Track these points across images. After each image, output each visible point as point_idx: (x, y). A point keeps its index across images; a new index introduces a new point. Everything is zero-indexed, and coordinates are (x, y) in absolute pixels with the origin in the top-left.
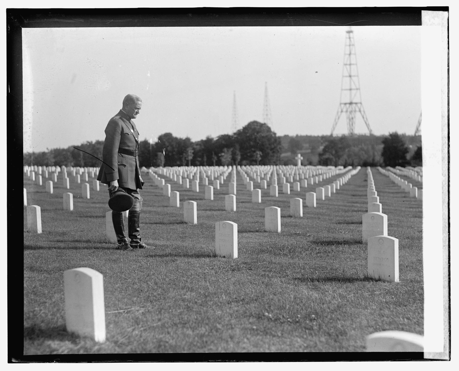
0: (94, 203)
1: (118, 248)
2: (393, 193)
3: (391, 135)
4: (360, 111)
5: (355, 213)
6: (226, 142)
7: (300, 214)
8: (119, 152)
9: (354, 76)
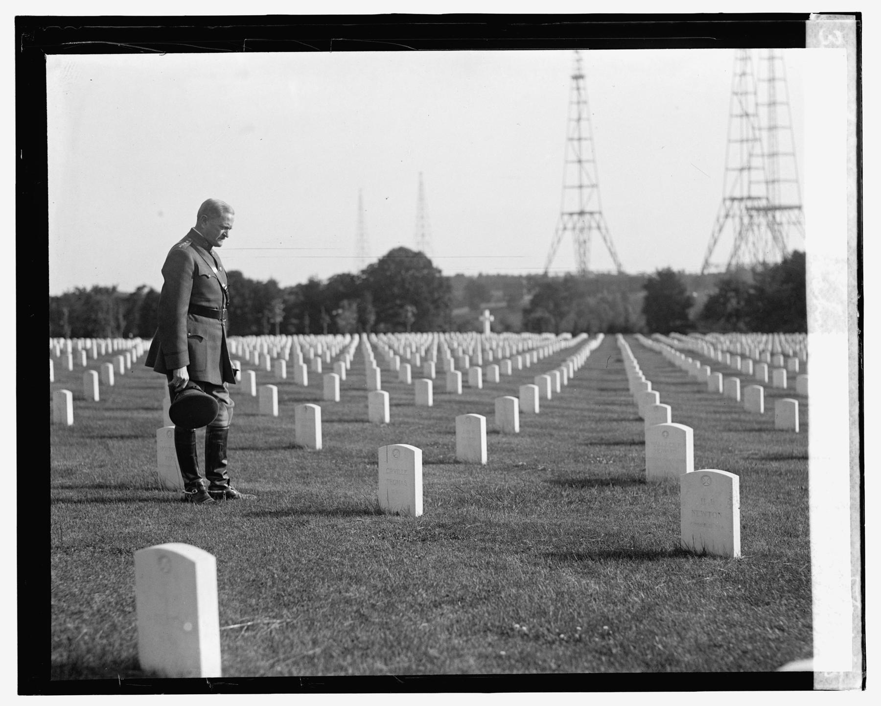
0: (107, 409)
1: (185, 500)
2: (674, 384)
3: (660, 274)
4: (599, 228)
5: (615, 423)
6: (344, 288)
7: (514, 428)
8: (190, 311)
9: (588, 161)
